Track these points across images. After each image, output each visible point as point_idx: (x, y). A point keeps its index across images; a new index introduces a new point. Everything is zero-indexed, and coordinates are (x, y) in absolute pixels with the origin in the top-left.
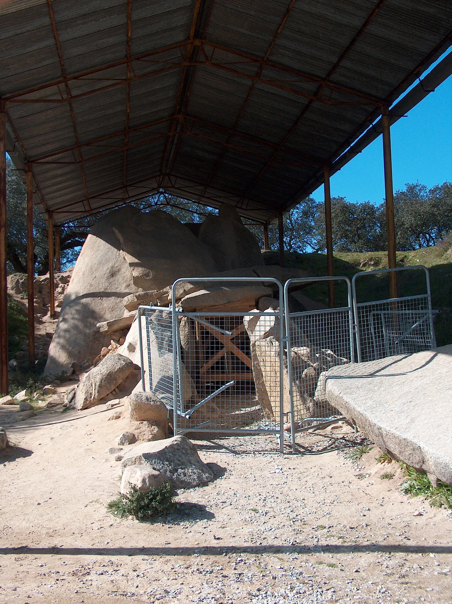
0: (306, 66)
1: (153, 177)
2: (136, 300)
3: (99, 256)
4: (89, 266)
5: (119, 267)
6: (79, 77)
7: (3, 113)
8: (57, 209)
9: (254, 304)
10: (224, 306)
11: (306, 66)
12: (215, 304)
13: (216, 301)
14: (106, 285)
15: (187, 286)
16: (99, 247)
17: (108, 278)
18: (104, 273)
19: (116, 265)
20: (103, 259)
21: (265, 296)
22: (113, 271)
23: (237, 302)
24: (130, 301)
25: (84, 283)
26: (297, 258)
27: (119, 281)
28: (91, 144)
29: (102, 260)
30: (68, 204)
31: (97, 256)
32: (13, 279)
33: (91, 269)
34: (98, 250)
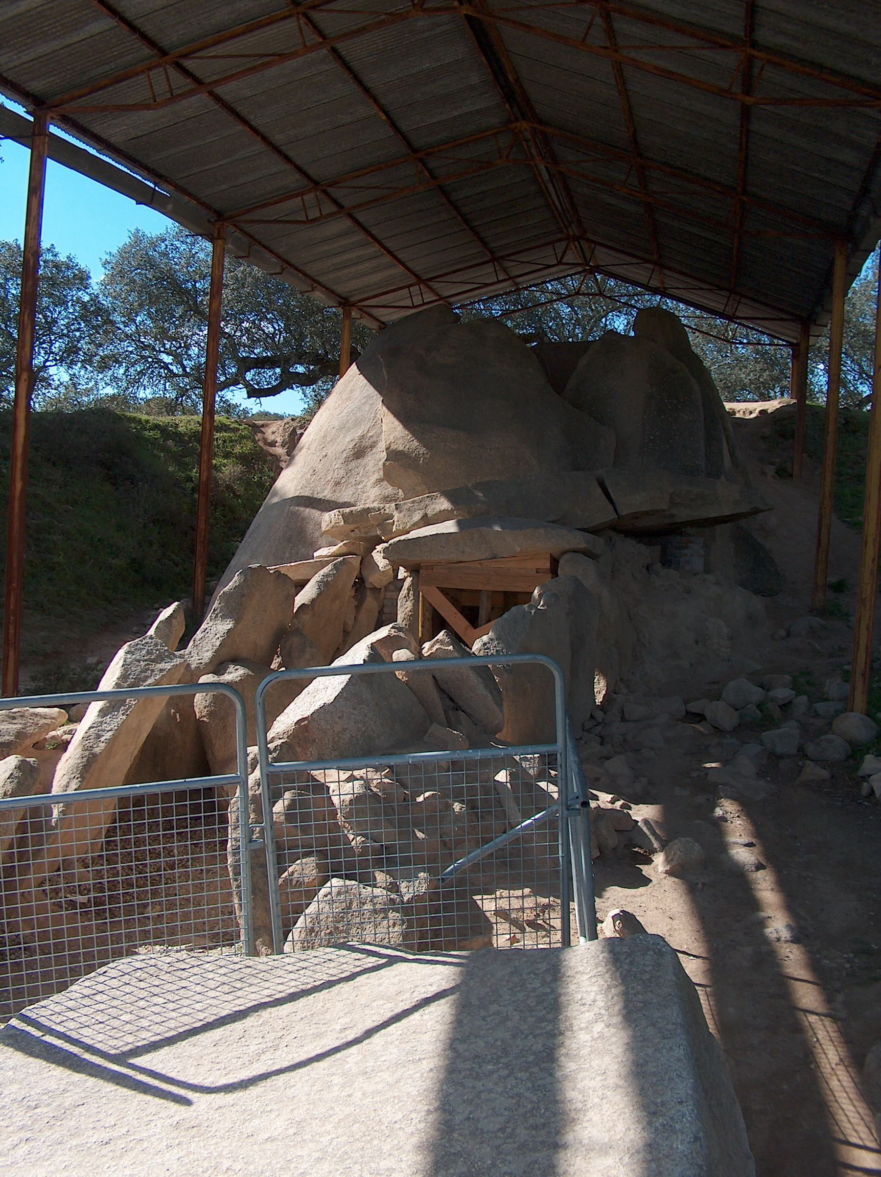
0: (693, 11)
1: (549, 244)
2: (342, 523)
3: (346, 411)
4: (323, 430)
5: (375, 439)
6: (194, 52)
7: (42, 137)
8: (361, 301)
9: (547, 565)
10: (480, 564)
11: (693, 11)
12: (460, 559)
13: (463, 552)
14: (340, 475)
15: (433, 506)
16: (352, 391)
17: (347, 461)
18: (344, 448)
19: (371, 434)
20: (351, 418)
21: (574, 552)
22: (360, 446)
23: (509, 559)
24: (332, 524)
25: (304, 467)
26: (847, 422)
27: (367, 469)
28: (339, 183)
29: (348, 421)
30: (381, 291)
31: (343, 411)
32: (287, 426)
33: (325, 437)
34: (349, 398)
